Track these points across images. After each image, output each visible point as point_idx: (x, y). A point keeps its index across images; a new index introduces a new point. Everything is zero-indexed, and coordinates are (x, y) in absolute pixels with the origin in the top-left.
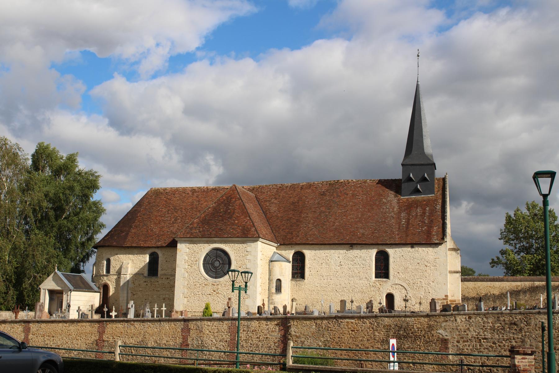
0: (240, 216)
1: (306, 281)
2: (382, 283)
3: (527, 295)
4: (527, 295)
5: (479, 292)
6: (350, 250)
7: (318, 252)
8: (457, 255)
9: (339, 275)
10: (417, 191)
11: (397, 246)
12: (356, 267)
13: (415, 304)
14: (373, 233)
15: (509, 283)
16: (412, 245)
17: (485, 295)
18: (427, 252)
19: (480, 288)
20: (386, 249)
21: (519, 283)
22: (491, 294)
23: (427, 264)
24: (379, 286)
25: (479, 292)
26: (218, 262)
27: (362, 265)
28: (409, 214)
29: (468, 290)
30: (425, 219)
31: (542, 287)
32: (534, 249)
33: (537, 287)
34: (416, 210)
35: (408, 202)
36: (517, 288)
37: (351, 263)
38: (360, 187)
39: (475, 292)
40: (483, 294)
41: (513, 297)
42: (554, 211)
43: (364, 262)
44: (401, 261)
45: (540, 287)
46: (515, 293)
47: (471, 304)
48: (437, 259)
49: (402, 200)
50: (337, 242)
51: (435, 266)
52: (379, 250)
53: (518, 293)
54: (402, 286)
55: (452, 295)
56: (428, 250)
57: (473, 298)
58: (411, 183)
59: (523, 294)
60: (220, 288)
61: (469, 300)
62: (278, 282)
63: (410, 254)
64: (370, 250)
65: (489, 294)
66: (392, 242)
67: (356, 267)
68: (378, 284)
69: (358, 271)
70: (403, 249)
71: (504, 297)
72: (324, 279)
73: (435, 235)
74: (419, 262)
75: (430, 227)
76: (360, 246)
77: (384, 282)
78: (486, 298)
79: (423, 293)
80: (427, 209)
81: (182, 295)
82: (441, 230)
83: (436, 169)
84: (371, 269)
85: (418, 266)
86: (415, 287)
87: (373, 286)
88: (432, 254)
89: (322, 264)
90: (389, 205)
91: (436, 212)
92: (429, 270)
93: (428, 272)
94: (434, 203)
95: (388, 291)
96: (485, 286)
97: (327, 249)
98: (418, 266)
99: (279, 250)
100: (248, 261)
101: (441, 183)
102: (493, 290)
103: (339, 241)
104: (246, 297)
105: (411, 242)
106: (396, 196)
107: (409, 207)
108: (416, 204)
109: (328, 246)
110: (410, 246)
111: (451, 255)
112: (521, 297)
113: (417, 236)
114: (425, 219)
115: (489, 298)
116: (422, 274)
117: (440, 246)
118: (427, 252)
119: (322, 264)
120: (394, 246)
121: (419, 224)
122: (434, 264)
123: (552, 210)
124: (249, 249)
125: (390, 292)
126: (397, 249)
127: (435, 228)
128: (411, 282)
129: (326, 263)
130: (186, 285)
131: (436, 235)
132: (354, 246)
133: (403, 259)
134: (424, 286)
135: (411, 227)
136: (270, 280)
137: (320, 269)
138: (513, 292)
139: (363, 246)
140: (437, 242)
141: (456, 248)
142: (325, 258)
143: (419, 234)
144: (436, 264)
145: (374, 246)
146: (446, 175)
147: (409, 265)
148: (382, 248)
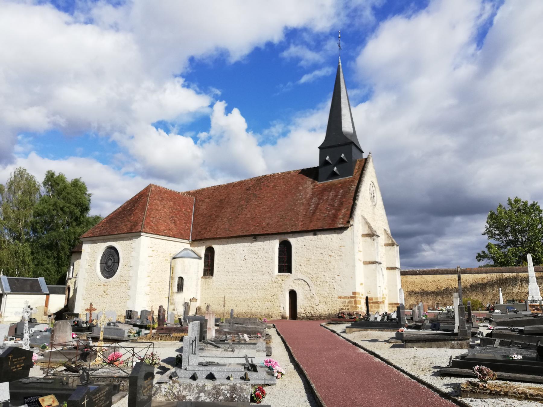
0: (138, 212)
1: (214, 278)
2: (284, 279)
3: (495, 288)
4: (495, 288)
5: (439, 286)
6: (253, 242)
7: (225, 246)
8: (372, 241)
9: (244, 270)
10: (334, 175)
11: (307, 234)
12: (259, 260)
13: (318, 303)
14: (278, 222)
15: (472, 275)
16: (315, 232)
17: (446, 289)
18: (331, 239)
19: (440, 281)
20: (288, 239)
21: (484, 275)
22: (452, 288)
23: (331, 253)
24: (281, 282)
25: (439, 286)
26: (111, 261)
27: (265, 258)
28: (320, 199)
29: (427, 284)
30: (335, 203)
31: (512, 279)
32: (520, 242)
33: (506, 279)
34: (328, 194)
35: (323, 186)
36: (482, 281)
37: (255, 256)
38: (283, 178)
39: (434, 286)
40: (443, 288)
41: (478, 291)
42: (538, 204)
43: (266, 255)
44: (303, 251)
45: (510, 279)
46: (481, 286)
47: (431, 299)
48: (342, 248)
49: (318, 186)
50: (241, 234)
51: (340, 256)
52: (281, 241)
53: (484, 287)
54: (304, 281)
55: (368, 292)
56: (332, 237)
57: (433, 292)
58: (328, 167)
59: (490, 288)
60: (109, 288)
61: (429, 294)
62: (180, 281)
63: (312, 242)
64: (272, 241)
65: (450, 288)
66: (294, 230)
67: (259, 260)
68: (280, 279)
69: (261, 266)
70: (305, 237)
71: (468, 291)
72: (230, 276)
73: (341, 219)
74: (322, 251)
75: (338, 210)
76: (263, 237)
77: (286, 277)
78: (447, 292)
79: (327, 290)
80: (341, 191)
81: (81, 296)
82: (349, 212)
83: (363, 152)
84: (273, 263)
85: (321, 257)
86: (319, 282)
87: (275, 282)
88: (337, 241)
89: (228, 259)
90: (303, 192)
91: (350, 193)
92: (334, 261)
93: (332, 263)
94: (350, 185)
95: (291, 288)
96: (446, 279)
97: (234, 243)
98: (321, 257)
99: (192, 247)
100: (132, 258)
101: (363, 164)
102: (454, 283)
103: (243, 233)
104: (128, 298)
105: (312, 229)
106: (313, 182)
107: (324, 190)
108: (331, 187)
109: (234, 239)
110: (312, 233)
111: (365, 242)
112: (488, 291)
113: (321, 221)
114: (335, 203)
115: (451, 293)
116: (326, 266)
117: (345, 231)
118: (331, 239)
119: (228, 259)
120: (296, 235)
121: (328, 208)
122: (339, 253)
123: (535, 203)
124: (133, 245)
125: (292, 288)
126: (299, 238)
127: (343, 211)
128: (314, 276)
129: (233, 258)
130: (85, 286)
131: (342, 218)
132: (258, 238)
133: (305, 248)
134: (328, 281)
135: (318, 212)
136: (171, 278)
137: (226, 264)
138: (478, 286)
139: (266, 236)
140: (341, 226)
141: (371, 233)
142: (231, 252)
143: (324, 218)
144: (341, 253)
145: (276, 236)
146: (369, 154)
147: (312, 255)
148: (284, 238)
